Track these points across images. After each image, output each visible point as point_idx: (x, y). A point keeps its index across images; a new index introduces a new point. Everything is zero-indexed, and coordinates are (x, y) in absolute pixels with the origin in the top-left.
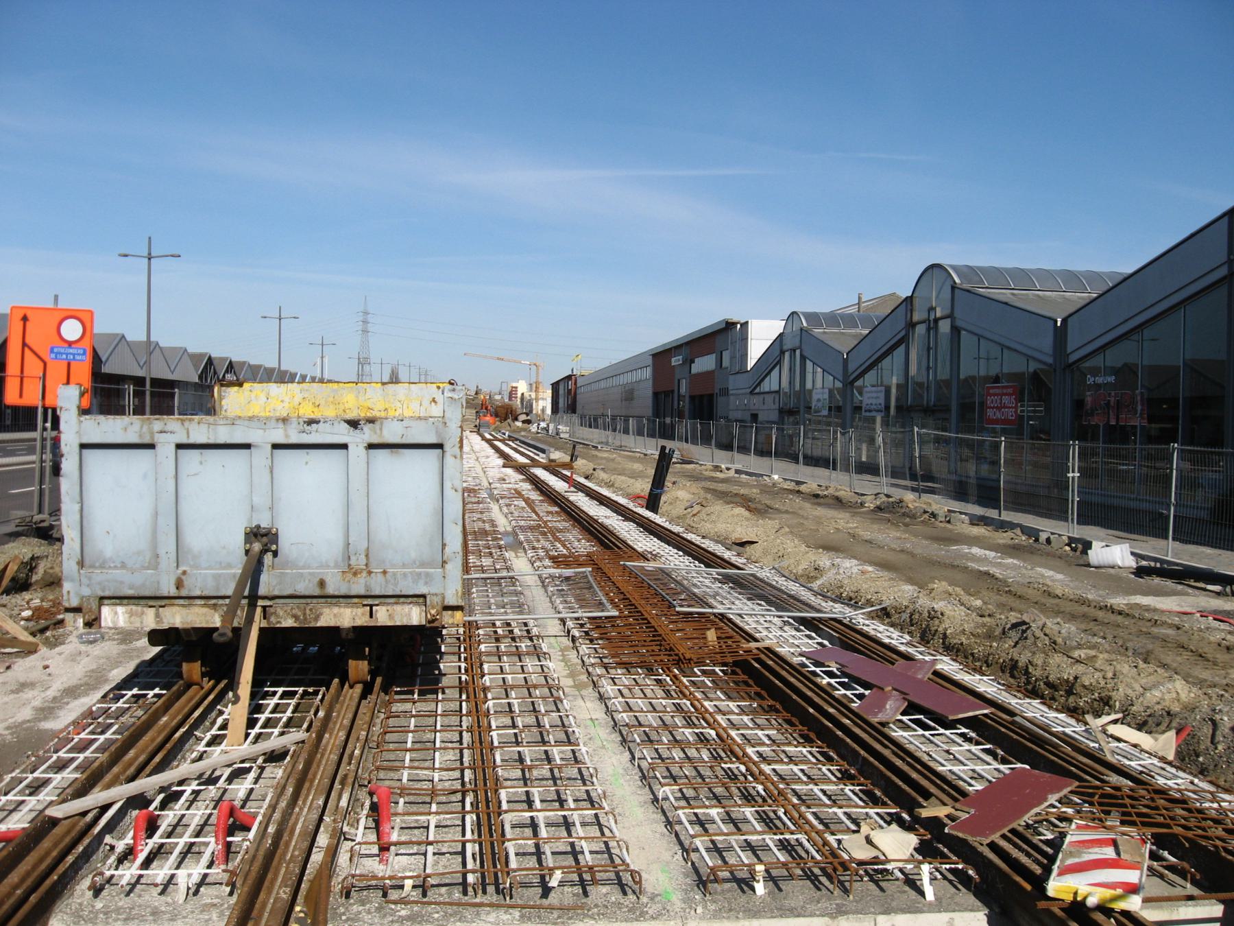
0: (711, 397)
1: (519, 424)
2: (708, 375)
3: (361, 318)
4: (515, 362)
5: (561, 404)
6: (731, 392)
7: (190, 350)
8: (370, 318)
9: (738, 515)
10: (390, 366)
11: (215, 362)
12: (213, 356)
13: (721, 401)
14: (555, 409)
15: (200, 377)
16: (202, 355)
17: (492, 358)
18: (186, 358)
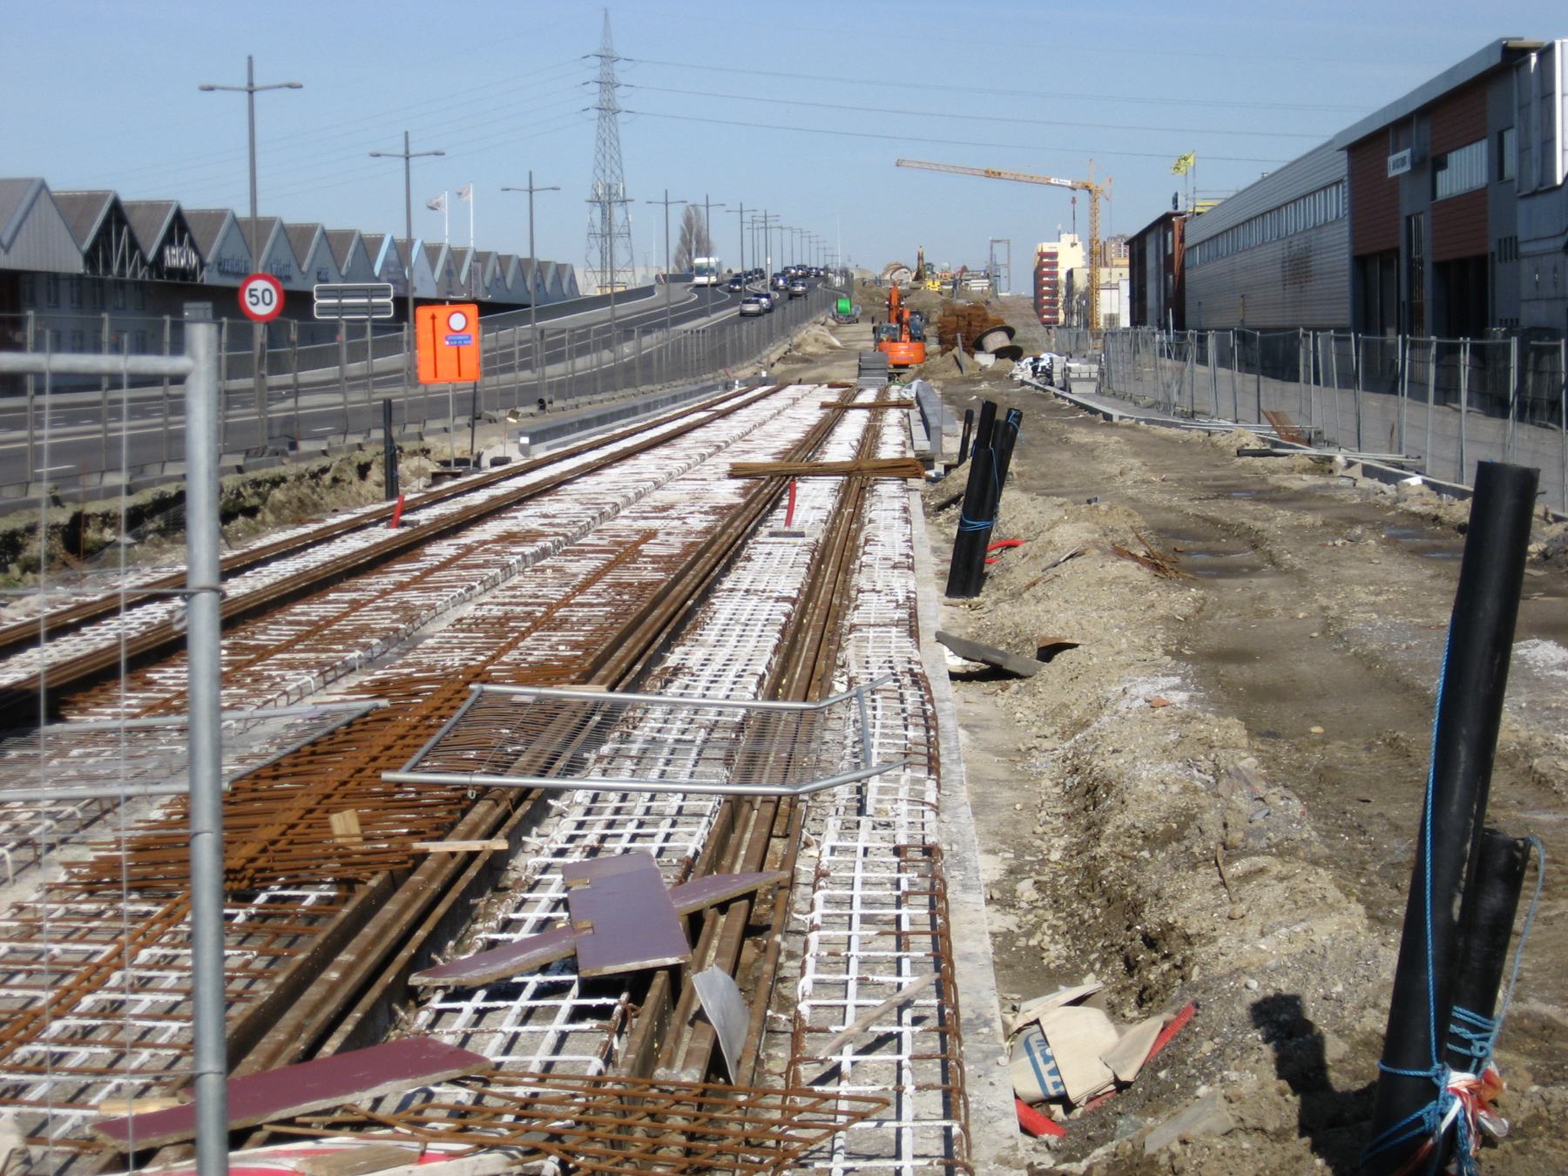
0: (1481, 262)
1: (986, 360)
2: (1473, 200)
3: (595, 74)
4: (1032, 181)
5: (1151, 301)
6: (1523, 249)
7: (58, 185)
8: (621, 72)
9: (1114, 581)
10: (682, 207)
11: (134, 219)
12: (126, 197)
13: (1501, 273)
14: (1138, 316)
15: (90, 258)
16: (93, 199)
17: (973, 172)
18: (44, 208)
